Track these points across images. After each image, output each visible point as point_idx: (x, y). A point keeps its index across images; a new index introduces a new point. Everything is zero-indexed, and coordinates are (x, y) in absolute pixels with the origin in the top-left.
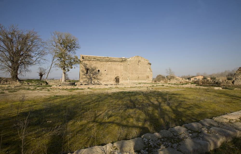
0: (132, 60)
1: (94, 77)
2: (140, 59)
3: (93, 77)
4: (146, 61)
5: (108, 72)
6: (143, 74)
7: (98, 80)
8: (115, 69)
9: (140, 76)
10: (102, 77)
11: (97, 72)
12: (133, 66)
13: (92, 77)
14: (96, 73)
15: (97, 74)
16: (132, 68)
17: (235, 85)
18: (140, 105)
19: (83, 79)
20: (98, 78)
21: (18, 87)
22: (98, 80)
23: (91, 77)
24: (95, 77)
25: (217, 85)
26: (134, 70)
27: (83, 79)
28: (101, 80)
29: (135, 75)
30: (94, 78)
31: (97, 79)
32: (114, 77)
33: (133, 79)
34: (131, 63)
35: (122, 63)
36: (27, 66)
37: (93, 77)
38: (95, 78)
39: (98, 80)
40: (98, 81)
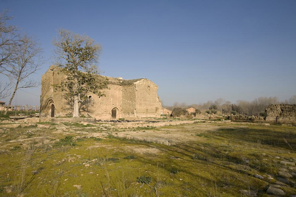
0: (140, 84)
1: (84, 107)
2: (149, 83)
3: (82, 109)
4: (156, 87)
5: (102, 100)
7: (89, 112)
8: (113, 96)
9: (149, 108)
12: (142, 93)
15: (87, 103)
17: (267, 121)
20: (88, 110)
21: (152, 147)
22: (88, 113)
24: (85, 108)
25: (250, 121)
26: (143, 98)
27: (67, 111)
30: (83, 110)
31: (88, 111)
32: (110, 109)
36: (100, 95)
37: (82, 107)
39: (89, 114)
40: (88, 115)
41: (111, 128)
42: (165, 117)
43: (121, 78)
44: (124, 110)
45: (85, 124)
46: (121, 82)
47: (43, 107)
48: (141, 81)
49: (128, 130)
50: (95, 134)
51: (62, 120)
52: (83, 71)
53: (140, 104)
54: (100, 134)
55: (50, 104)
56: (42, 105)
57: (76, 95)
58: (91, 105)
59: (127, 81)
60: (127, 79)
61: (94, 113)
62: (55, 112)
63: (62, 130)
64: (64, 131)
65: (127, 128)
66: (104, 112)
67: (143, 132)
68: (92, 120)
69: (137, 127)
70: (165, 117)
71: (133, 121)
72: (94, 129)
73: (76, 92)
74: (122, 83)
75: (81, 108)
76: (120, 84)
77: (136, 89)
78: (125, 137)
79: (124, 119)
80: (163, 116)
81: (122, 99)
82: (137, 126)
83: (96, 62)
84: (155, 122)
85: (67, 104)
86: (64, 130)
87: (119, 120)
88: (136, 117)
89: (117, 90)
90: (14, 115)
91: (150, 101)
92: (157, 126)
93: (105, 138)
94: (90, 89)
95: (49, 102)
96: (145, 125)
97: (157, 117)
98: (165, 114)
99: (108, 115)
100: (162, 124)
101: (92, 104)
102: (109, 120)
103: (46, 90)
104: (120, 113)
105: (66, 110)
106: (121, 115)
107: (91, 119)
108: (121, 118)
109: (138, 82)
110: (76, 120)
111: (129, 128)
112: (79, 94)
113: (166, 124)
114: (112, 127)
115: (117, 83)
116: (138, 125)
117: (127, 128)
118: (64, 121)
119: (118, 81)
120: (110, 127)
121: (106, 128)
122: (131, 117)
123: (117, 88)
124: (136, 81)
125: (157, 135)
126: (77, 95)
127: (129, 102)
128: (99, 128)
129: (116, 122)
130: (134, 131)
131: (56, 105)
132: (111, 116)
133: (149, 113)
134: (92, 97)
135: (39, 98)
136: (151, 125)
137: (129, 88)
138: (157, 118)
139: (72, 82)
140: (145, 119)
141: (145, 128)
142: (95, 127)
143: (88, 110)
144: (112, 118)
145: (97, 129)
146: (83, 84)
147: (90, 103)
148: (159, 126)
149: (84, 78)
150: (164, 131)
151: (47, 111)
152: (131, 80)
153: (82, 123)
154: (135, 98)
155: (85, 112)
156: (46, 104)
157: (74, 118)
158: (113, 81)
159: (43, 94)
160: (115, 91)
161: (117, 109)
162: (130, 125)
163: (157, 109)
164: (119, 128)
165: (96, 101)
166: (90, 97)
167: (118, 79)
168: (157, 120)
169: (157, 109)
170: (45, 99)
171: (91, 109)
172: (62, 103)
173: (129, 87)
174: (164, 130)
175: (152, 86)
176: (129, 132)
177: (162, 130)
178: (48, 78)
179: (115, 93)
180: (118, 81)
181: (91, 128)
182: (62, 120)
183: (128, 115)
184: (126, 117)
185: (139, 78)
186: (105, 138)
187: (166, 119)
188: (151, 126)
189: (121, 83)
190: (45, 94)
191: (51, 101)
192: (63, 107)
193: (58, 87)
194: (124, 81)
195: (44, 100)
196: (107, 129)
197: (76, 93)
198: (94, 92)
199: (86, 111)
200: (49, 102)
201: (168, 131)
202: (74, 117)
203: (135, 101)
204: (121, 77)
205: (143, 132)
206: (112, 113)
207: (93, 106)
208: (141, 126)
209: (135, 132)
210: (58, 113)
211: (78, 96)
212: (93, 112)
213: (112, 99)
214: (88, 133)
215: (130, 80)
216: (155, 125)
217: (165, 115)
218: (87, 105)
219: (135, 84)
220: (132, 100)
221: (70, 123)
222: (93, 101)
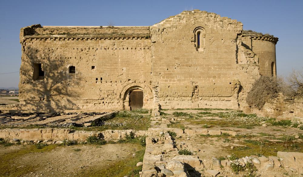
6: (215, 77)
7: (70, 95)
13: (50, 90)
22: (68, 98)
23: (48, 89)
28: (77, 96)
31: (67, 94)
37: (55, 87)
39: (70, 98)
75: (53, 88)
105: (24, 92)
143: (66, 91)
199: (63, 94)
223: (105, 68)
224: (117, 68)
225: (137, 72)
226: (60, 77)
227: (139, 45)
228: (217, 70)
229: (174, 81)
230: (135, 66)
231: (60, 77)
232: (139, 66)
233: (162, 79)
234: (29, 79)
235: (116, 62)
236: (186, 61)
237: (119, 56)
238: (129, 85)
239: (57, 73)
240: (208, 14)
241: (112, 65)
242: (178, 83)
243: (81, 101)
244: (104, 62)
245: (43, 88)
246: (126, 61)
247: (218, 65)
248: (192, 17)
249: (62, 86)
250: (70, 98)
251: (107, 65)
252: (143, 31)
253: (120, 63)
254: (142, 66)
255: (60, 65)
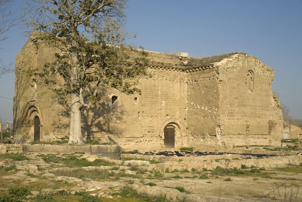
0: (230, 66)
4: (268, 73)
5: (142, 106)
6: (259, 117)
7: (111, 133)
8: (166, 96)
9: (252, 122)
10: (125, 122)
11: (108, 104)
12: (234, 88)
13: (91, 125)
14: (104, 108)
16: (231, 96)
18: (227, 200)
19: (63, 130)
20: (111, 129)
22: (110, 135)
23: (89, 124)
24: (102, 123)
27: (63, 130)
28: (119, 133)
29: (238, 119)
30: (99, 128)
31: (109, 131)
32: (160, 125)
33: (234, 135)
34: (229, 79)
35: (185, 73)
37: (96, 122)
38: (101, 128)
39: (112, 137)
40: (110, 139)
41: (146, 171)
42: (292, 144)
43: (185, 55)
44: (192, 128)
45: (92, 159)
46: (186, 63)
47: (18, 121)
48: (231, 59)
49: (190, 175)
50: (92, 186)
51: (42, 150)
52: (89, 37)
53: (231, 114)
54: (105, 185)
55: (30, 115)
56: (17, 118)
57: (74, 91)
58: (117, 118)
59: (198, 59)
60: (199, 56)
61: (124, 134)
62: (42, 132)
63: (25, 172)
64: (29, 175)
65: (190, 169)
66: (147, 133)
67: (226, 180)
68: (109, 151)
69: (215, 167)
70: (292, 144)
71: (211, 153)
72: (106, 170)
73: (74, 86)
74: (186, 65)
75: (94, 123)
76: (183, 67)
77: (221, 77)
78: (163, 196)
79: (191, 149)
80: (290, 142)
81: (187, 102)
82: (215, 165)
83: (120, 15)
84: (265, 155)
85: (64, 116)
86: (32, 172)
87: (179, 151)
88: (221, 144)
89: (175, 81)
90: (186, 150)
91: (255, 106)
92: (267, 166)
93: (111, 197)
94: (105, 78)
95: (30, 111)
96: (236, 165)
97: (272, 144)
98: (294, 137)
99: (155, 139)
100: (282, 161)
101: (120, 115)
102: (157, 152)
103: (24, 86)
104: (184, 135)
105: (61, 128)
106: (185, 140)
107: (107, 148)
108: (185, 145)
109: (225, 61)
110: (73, 149)
111: (193, 170)
112: (81, 90)
113: (291, 162)
114: (151, 167)
115: (176, 65)
116: (218, 164)
117: (190, 169)
118: (48, 151)
119: (178, 62)
120: (144, 168)
121: (133, 169)
122: (209, 143)
123: (175, 76)
124: (220, 59)
125: (260, 190)
126: (76, 91)
127: (203, 108)
128: (117, 169)
129: (172, 155)
130: (204, 177)
131: (42, 117)
132: (163, 143)
133: (252, 136)
134: (118, 98)
135: (12, 104)
136: (250, 163)
137: (203, 77)
138: (271, 148)
139: (65, 63)
140: (241, 148)
141: (237, 172)
142: (107, 167)
143: (109, 128)
144: (164, 146)
145: (110, 172)
146: (88, 66)
147: (114, 112)
148: (273, 166)
149: (90, 51)
150: (283, 179)
151: (25, 130)
152: (208, 58)
153: (85, 156)
154: (217, 98)
155: (103, 132)
156: (24, 115)
157: (70, 145)
158: (165, 62)
159: (17, 95)
160: (171, 85)
161: (177, 125)
162: (196, 162)
163: (271, 125)
164: (167, 171)
165: (127, 107)
166: (114, 98)
167: (178, 57)
168: (270, 152)
169: (271, 125)
170: (22, 104)
171: (116, 125)
172: (53, 113)
173: (204, 73)
174: (283, 176)
175: (258, 70)
176: (188, 180)
177: (279, 176)
178: (26, 59)
179: (171, 89)
180: (178, 62)
181: (98, 168)
182: (42, 150)
183: (202, 140)
184: (198, 143)
185: (226, 53)
186: (113, 195)
187: (294, 148)
188: (252, 167)
189: (184, 65)
190: (22, 94)
191: (32, 108)
192: (55, 122)
193: (38, 76)
194: (193, 60)
195: (20, 107)
196: (137, 173)
197: (75, 88)
198: (113, 84)
199: (104, 131)
200: (30, 111)
201: (294, 179)
202: (70, 142)
203: (218, 107)
204: (185, 52)
205: (226, 180)
206: (165, 136)
207: (120, 119)
208: (223, 166)
209: (204, 181)
210: (46, 135)
211: (79, 94)
212: (120, 134)
213: (164, 102)
214: (80, 180)
215: (206, 57)
216: (262, 163)
217: (294, 141)
218: (107, 116)
219: (218, 67)
220: (211, 104)
221: (58, 157)
222: (120, 107)
223: (147, 101)
224: (157, 102)
225: (173, 107)
226: (101, 109)
227: (176, 78)
228: (261, 110)
229: (235, 119)
230: (173, 101)
231: (101, 109)
232: (176, 101)
233: (227, 117)
234: (67, 110)
235: (157, 94)
236: (242, 101)
237: (160, 88)
238: (167, 121)
239: (99, 104)
240: (256, 59)
241: (153, 98)
242: (237, 122)
243: (124, 138)
244: (146, 94)
245: (84, 122)
246: (165, 95)
247: (261, 106)
248: (246, 61)
249: (104, 120)
250: (112, 137)
251: (148, 98)
252: (168, 60)
253: (160, 95)
254: (178, 101)
255: (102, 94)
